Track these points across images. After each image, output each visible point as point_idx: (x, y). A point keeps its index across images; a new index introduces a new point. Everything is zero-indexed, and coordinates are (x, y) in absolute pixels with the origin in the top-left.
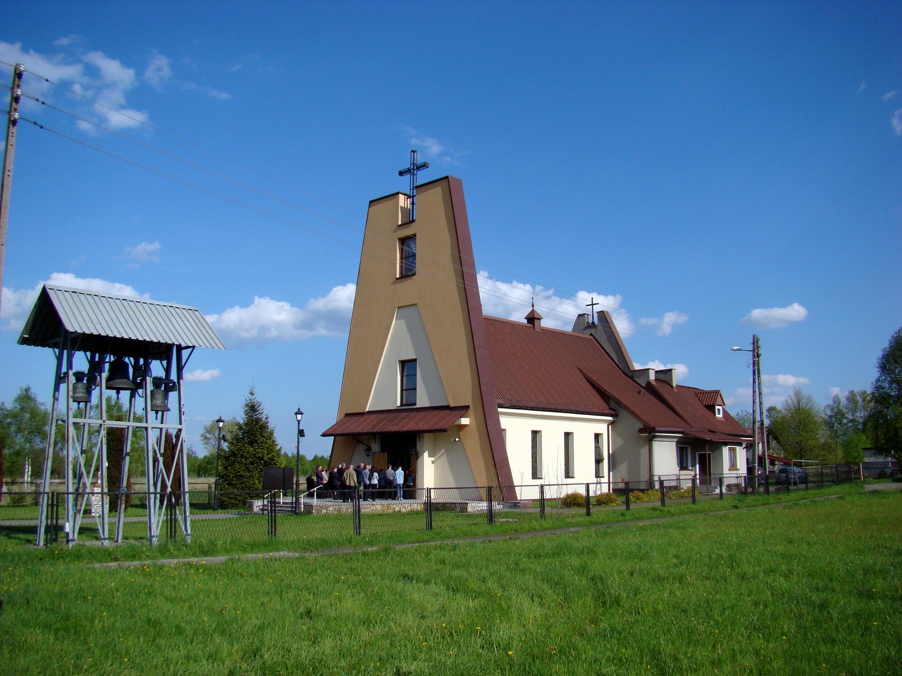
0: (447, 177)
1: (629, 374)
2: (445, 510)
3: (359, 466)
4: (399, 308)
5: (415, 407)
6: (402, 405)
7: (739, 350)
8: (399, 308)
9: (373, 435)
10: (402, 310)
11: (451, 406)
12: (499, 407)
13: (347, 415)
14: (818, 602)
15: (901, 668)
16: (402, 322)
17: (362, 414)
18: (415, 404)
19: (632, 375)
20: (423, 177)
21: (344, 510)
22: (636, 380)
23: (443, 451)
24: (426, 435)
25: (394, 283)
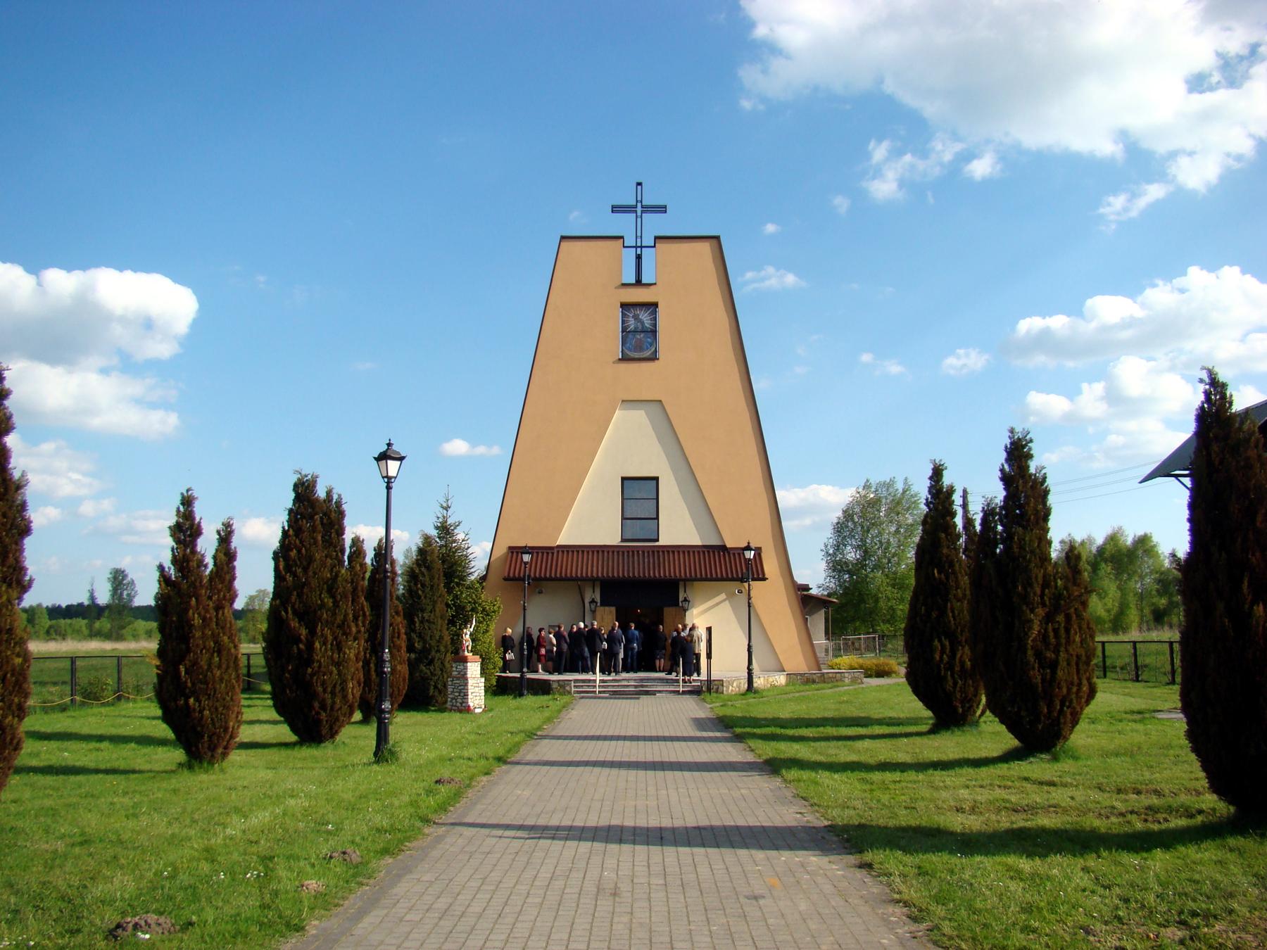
4: (623, 401)
5: (657, 544)
8: (623, 401)
9: (593, 581)
18: (657, 540)
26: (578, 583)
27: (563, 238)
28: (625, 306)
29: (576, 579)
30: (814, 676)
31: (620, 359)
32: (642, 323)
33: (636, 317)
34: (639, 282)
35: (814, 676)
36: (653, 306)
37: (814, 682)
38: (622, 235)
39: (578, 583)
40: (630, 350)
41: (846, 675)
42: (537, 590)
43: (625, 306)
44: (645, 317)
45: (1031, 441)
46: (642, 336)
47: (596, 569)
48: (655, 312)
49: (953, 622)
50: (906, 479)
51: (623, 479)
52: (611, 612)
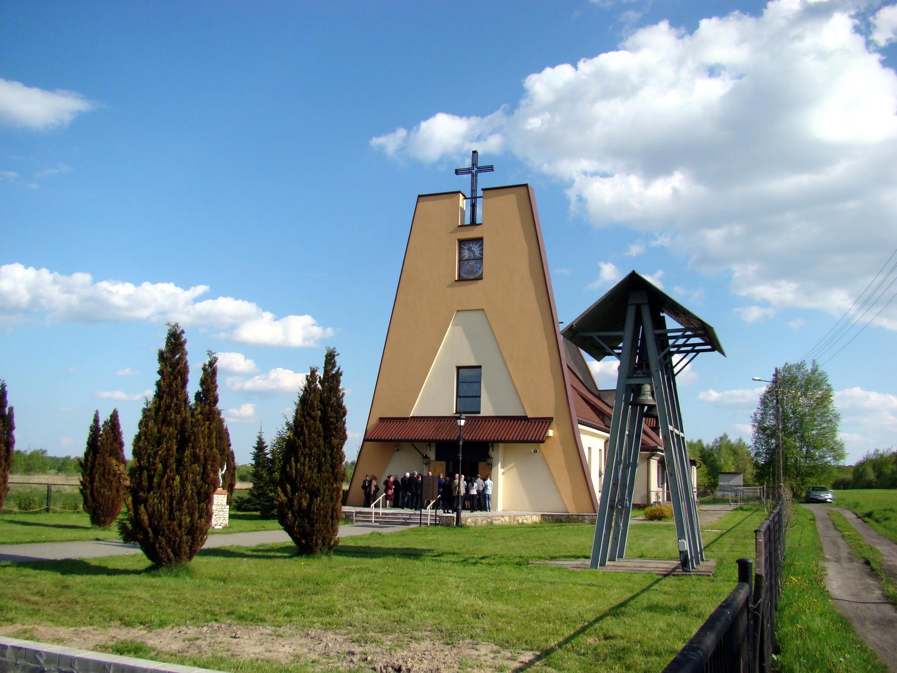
0: (526, 185)
1: (596, 393)
2: (569, 522)
3: (414, 474)
4: (457, 311)
5: (478, 415)
6: (457, 413)
7: (759, 380)
8: (457, 311)
9: (429, 442)
10: (460, 314)
11: (529, 417)
12: (579, 423)
13: (381, 419)
14: (458, 607)
15: (501, 669)
16: (459, 329)
17: (407, 419)
18: (479, 413)
19: (599, 394)
20: (485, 180)
21: (480, 522)
22: (605, 401)
23: (513, 464)
24: (501, 445)
25: (451, 286)
26: (415, 443)
27: (420, 196)
28: (462, 242)
29: (394, 441)
30: (562, 517)
31: (456, 281)
32: (474, 253)
33: (469, 249)
34: (473, 223)
35: (562, 517)
36: (479, 240)
37: (561, 521)
38: (524, 183)
39: (415, 443)
40: (465, 273)
41: (587, 517)
42: (396, 448)
43: (462, 242)
44: (475, 248)
45: (183, 332)
46: (473, 262)
47: (426, 432)
48: (482, 245)
49: (765, 486)
50: (814, 361)
51: (458, 368)
52: (442, 465)
